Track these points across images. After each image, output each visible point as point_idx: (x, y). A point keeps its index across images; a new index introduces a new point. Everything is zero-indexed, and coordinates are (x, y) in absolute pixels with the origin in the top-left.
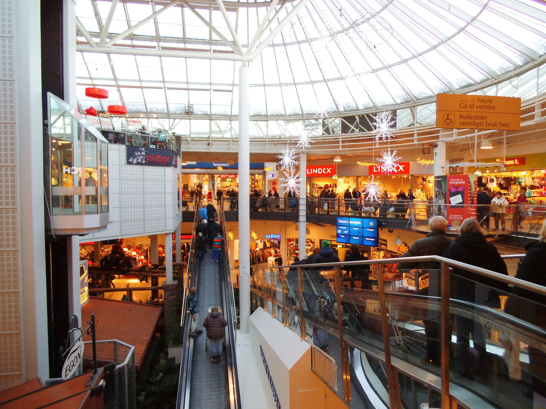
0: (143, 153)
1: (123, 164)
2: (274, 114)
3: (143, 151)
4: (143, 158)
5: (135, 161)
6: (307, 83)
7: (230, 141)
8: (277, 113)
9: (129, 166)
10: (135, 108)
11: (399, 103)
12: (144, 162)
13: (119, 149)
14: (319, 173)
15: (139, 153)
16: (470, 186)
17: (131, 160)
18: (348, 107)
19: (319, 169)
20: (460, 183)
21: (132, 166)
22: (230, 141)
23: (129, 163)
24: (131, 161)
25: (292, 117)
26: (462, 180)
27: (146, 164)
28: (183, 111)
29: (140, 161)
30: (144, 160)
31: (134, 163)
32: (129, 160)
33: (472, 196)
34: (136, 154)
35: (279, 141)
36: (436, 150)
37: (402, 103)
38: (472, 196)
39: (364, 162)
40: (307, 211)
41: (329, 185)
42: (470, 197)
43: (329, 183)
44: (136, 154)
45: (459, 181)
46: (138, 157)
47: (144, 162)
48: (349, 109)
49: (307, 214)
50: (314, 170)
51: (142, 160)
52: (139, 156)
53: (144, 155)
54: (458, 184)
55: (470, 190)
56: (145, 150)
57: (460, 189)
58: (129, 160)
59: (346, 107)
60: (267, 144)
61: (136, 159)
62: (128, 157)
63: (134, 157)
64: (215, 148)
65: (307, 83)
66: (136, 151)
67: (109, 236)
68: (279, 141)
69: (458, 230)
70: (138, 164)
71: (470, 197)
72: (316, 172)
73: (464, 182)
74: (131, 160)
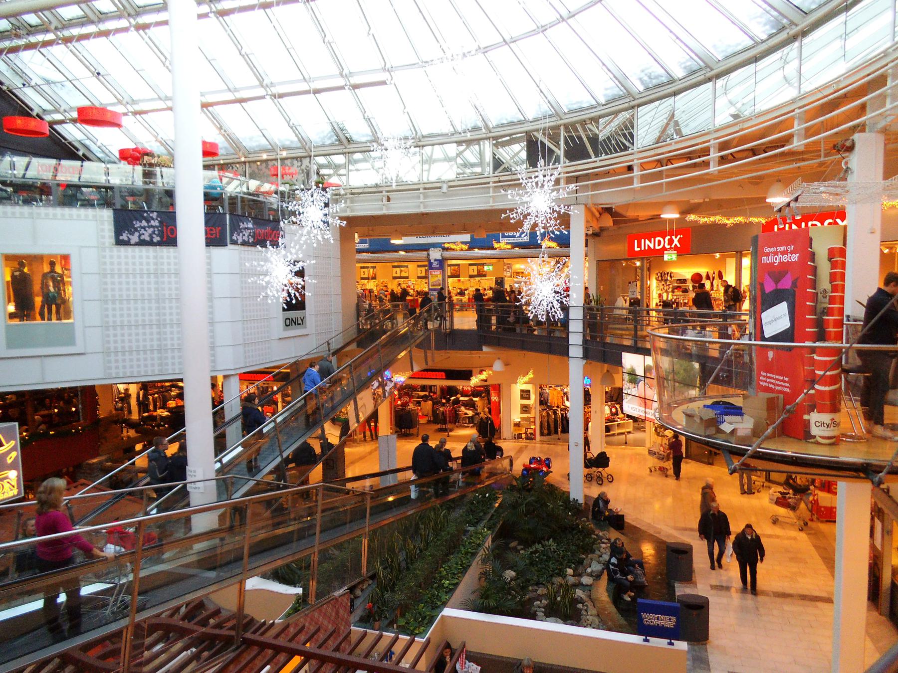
0: (155, 223)
1: (107, 245)
2: (505, 122)
3: (153, 219)
4: (154, 232)
5: (135, 238)
6: (533, 33)
7: (419, 189)
8: (510, 120)
9: (122, 249)
10: (257, 143)
11: (764, 37)
12: (156, 239)
13: (95, 216)
14: (657, 247)
15: (144, 223)
16: (814, 270)
17: (124, 237)
18: (650, 78)
19: (657, 239)
20: (785, 258)
21: (129, 249)
22: (419, 189)
23: (119, 242)
24: (126, 239)
25: (547, 120)
26: (791, 248)
27: (160, 244)
28: (333, 140)
29: (148, 239)
30: (157, 235)
31: (132, 242)
32: (121, 238)
33: (820, 307)
34: (242, 226)
35: (512, 180)
36: (854, 160)
37: (771, 36)
38: (820, 307)
39: (715, 215)
40: (584, 336)
41: (704, 275)
42: (813, 310)
43: (703, 271)
44: (137, 224)
45: (783, 253)
46: (143, 231)
47: (156, 239)
48: (655, 82)
49: (585, 341)
50: (647, 242)
51: (150, 235)
52: (144, 228)
53: (157, 227)
54: (781, 263)
55: (814, 284)
56: (158, 216)
57: (786, 283)
58: (121, 238)
59: (646, 78)
60: (491, 190)
61: (137, 234)
62: (118, 231)
63: (132, 230)
64: (401, 207)
65: (533, 33)
66: (136, 219)
67: (96, 377)
68: (512, 180)
69: (740, 433)
70: (142, 243)
71: (813, 310)
72: (652, 246)
73: (795, 257)
74: (124, 237)
